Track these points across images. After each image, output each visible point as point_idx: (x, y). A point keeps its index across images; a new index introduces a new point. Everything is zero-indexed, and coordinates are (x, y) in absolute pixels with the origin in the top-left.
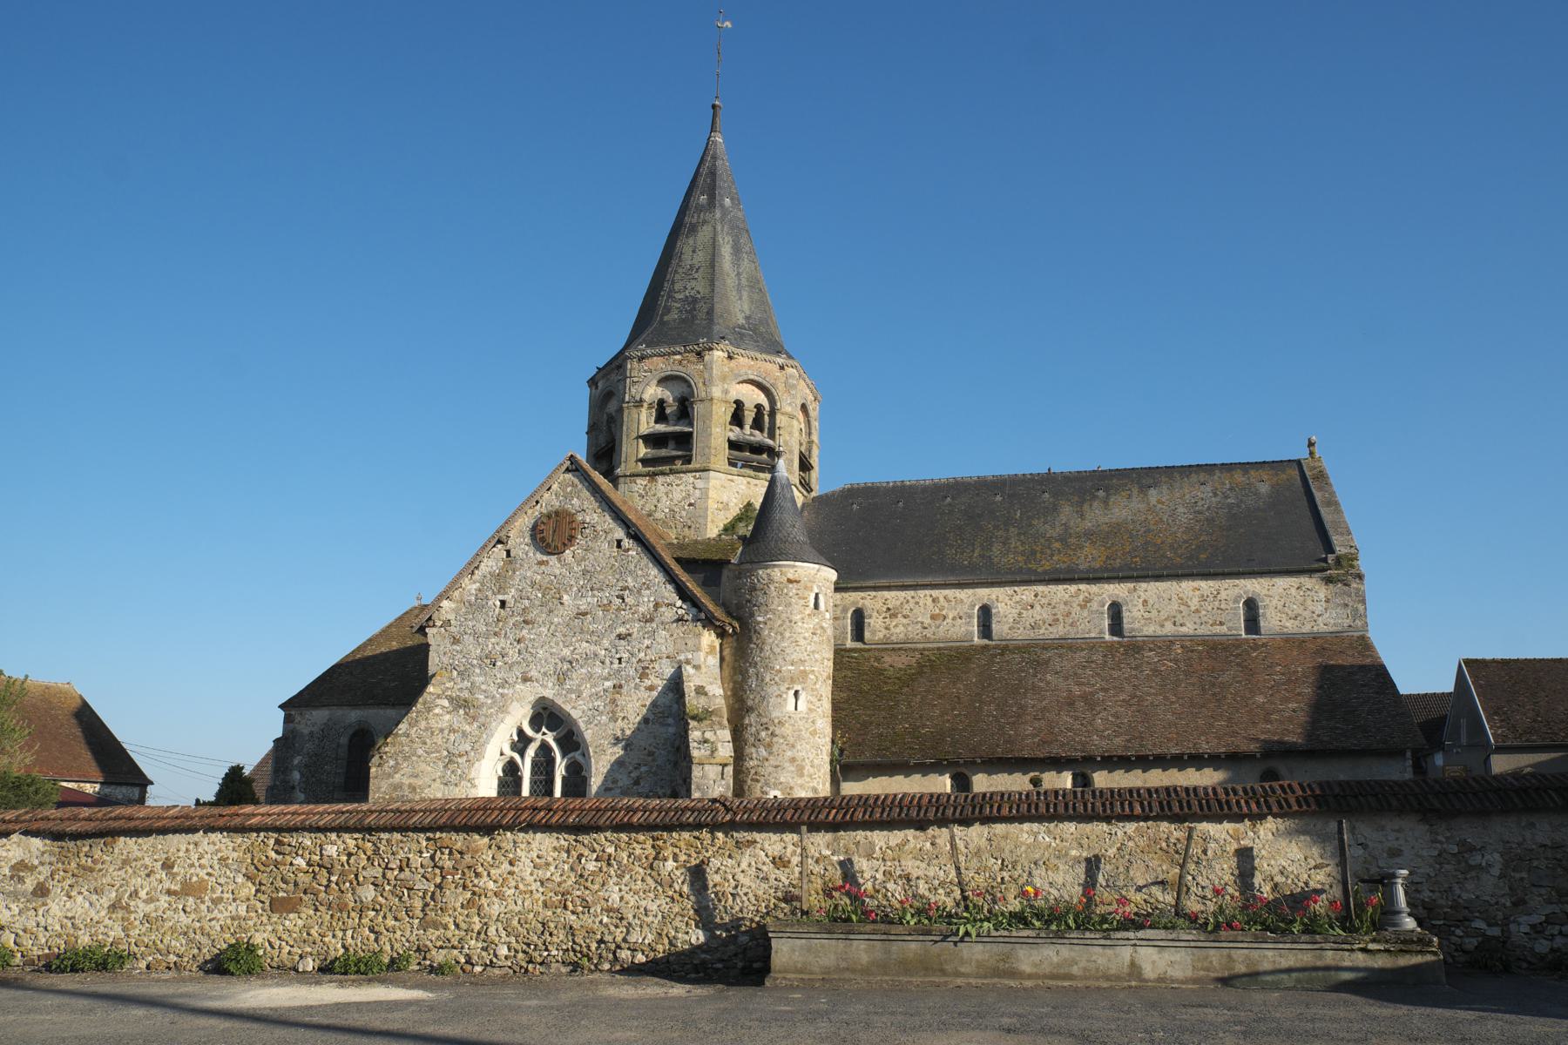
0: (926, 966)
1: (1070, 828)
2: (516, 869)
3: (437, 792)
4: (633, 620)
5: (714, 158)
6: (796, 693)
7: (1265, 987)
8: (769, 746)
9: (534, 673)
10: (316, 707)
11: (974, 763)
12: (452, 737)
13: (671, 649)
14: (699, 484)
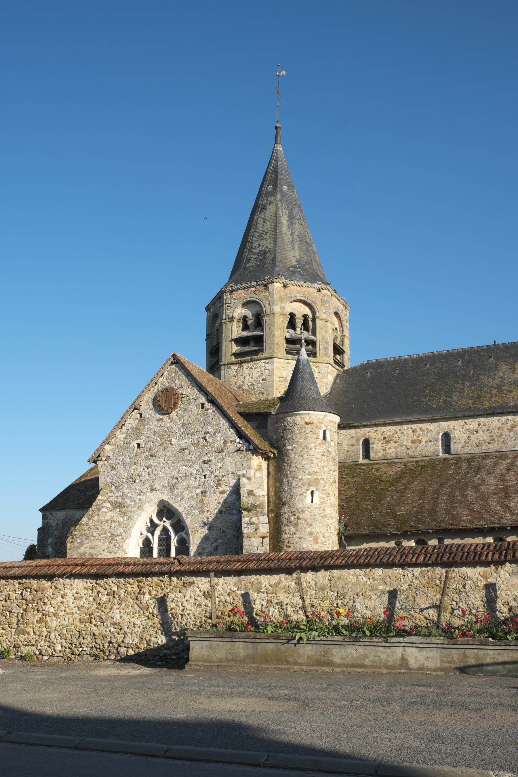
0: (278, 659)
1: (378, 571)
2: (64, 600)
3: (105, 555)
4: (211, 452)
5: (277, 161)
6: (312, 492)
7: (486, 674)
8: (296, 525)
9: (157, 486)
10: (58, 510)
11: (428, 533)
12: (113, 525)
14: (268, 366)
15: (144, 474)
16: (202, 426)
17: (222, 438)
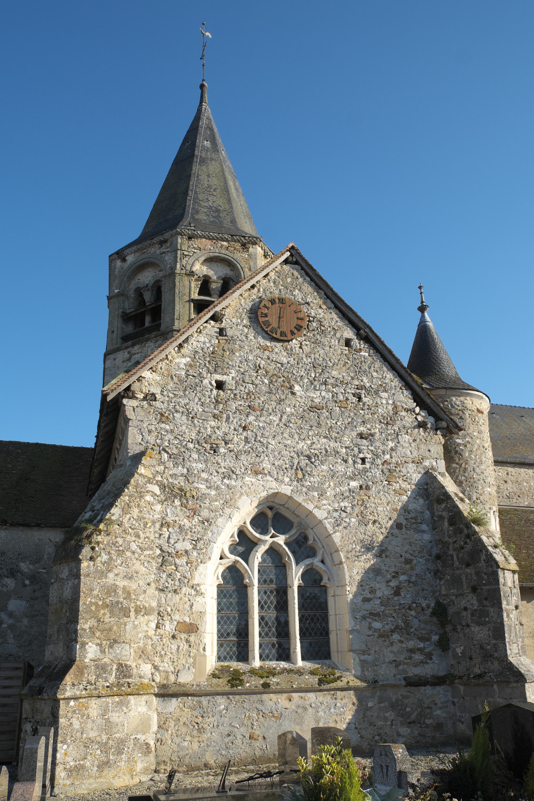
9: (266, 465)
13: (415, 454)
15: (236, 439)
16: (352, 374)
17: (391, 402)
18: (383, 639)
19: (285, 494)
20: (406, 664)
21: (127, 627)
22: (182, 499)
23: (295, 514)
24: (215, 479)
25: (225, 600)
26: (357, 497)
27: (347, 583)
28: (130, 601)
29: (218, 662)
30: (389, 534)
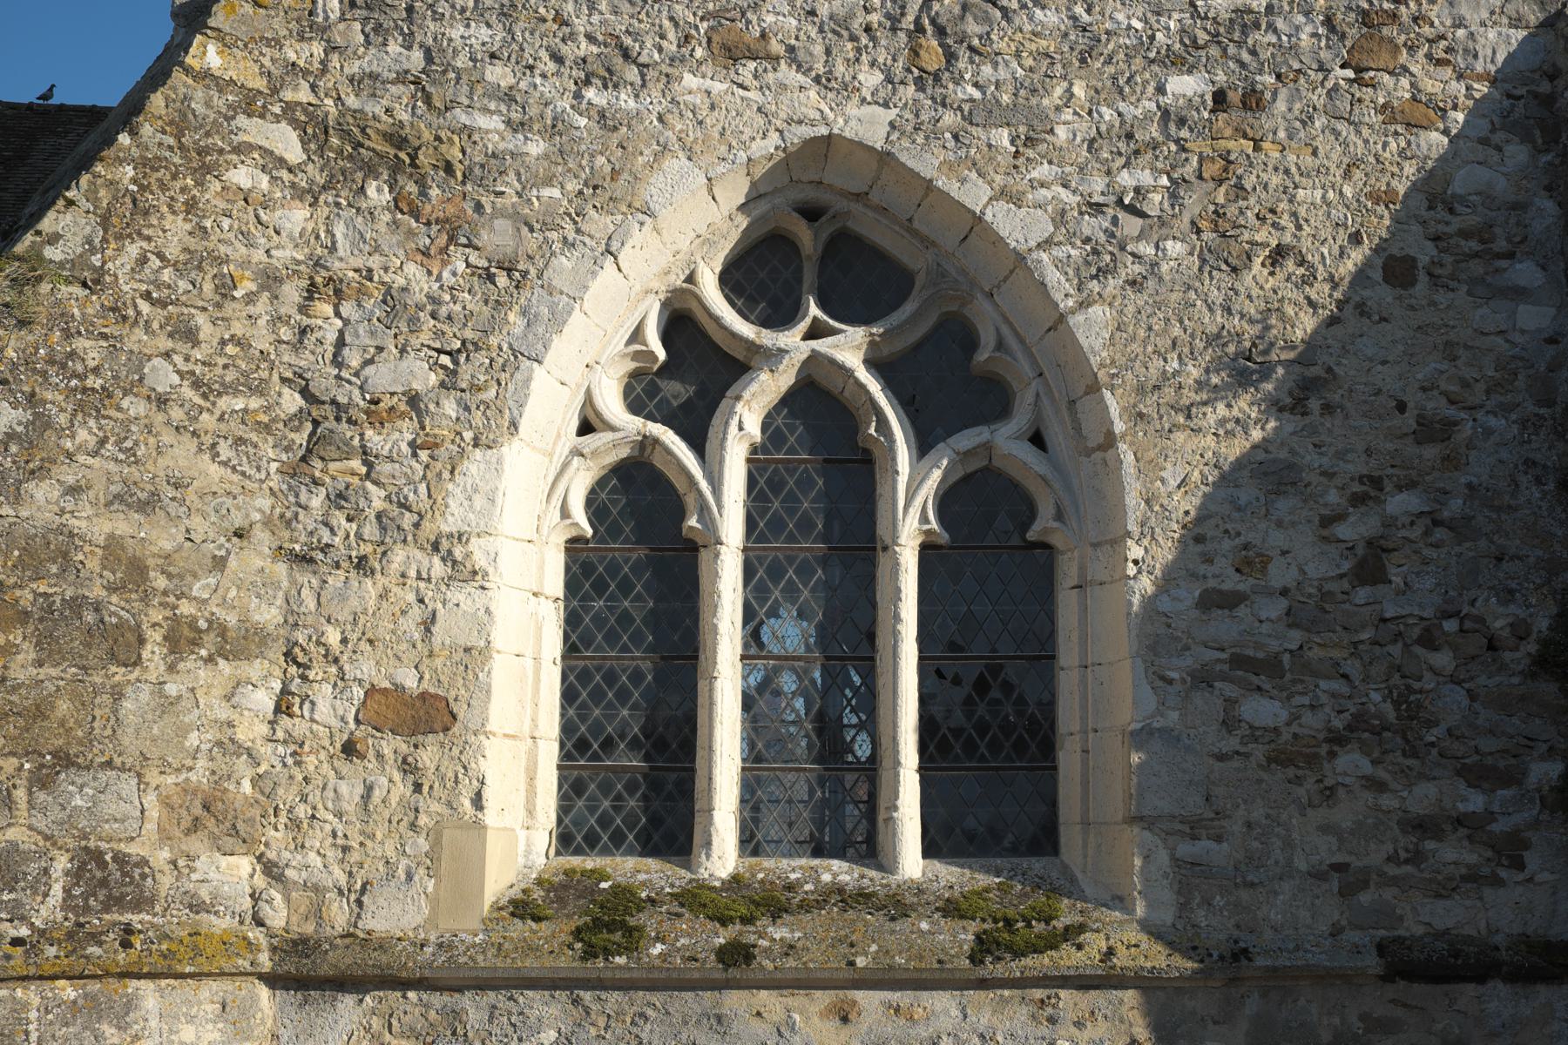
18: (1291, 772)
19: (860, 144)
20: (1395, 881)
21: (127, 704)
22: (401, 180)
23: (915, 233)
24: (546, 89)
25: (598, 604)
26: (1199, 146)
27: (1133, 527)
28: (145, 599)
29: (558, 853)
30: (1349, 309)
